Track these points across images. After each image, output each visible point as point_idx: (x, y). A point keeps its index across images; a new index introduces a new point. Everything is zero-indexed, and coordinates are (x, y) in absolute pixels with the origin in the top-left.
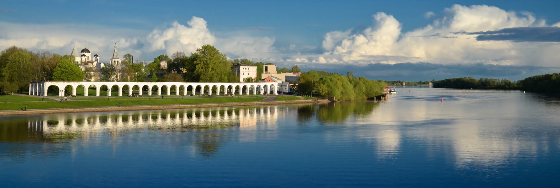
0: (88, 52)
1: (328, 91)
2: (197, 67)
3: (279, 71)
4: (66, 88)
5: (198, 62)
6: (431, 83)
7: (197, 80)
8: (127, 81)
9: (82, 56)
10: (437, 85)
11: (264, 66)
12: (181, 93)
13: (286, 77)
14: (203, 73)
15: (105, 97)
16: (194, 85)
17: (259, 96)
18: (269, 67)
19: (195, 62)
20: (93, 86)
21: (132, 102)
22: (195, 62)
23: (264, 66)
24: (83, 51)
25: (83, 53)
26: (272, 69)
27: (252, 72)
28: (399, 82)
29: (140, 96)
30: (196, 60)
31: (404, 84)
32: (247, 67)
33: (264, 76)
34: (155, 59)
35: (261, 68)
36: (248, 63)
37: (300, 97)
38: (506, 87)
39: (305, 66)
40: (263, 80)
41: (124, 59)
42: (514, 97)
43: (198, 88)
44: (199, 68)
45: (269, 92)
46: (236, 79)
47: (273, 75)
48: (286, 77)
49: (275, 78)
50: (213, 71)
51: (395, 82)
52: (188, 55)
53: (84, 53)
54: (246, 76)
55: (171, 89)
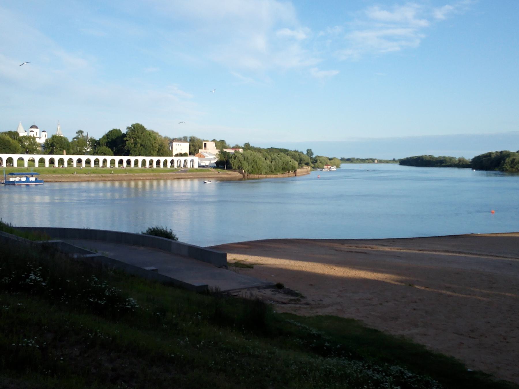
0: (37, 128)
2: (127, 143)
5: (128, 139)
7: (127, 154)
10: (404, 162)
11: (204, 143)
14: (133, 149)
15: (42, 168)
16: (125, 158)
17: (172, 168)
19: (125, 139)
20: (31, 159)
21: (48, 172)
22: (125, 139)
24: (32, 127)
25: (31, 129)
27: (185, 147)
28: (371, 159)
30: (126, 137)
31: (376, 161)
38: (461, 164)
41: (77, 135)
42: (469, 173)
43: (165, 162)
44: (130, 143)
51: (367, 159)
54: (178, 152)
55: (95, 161)
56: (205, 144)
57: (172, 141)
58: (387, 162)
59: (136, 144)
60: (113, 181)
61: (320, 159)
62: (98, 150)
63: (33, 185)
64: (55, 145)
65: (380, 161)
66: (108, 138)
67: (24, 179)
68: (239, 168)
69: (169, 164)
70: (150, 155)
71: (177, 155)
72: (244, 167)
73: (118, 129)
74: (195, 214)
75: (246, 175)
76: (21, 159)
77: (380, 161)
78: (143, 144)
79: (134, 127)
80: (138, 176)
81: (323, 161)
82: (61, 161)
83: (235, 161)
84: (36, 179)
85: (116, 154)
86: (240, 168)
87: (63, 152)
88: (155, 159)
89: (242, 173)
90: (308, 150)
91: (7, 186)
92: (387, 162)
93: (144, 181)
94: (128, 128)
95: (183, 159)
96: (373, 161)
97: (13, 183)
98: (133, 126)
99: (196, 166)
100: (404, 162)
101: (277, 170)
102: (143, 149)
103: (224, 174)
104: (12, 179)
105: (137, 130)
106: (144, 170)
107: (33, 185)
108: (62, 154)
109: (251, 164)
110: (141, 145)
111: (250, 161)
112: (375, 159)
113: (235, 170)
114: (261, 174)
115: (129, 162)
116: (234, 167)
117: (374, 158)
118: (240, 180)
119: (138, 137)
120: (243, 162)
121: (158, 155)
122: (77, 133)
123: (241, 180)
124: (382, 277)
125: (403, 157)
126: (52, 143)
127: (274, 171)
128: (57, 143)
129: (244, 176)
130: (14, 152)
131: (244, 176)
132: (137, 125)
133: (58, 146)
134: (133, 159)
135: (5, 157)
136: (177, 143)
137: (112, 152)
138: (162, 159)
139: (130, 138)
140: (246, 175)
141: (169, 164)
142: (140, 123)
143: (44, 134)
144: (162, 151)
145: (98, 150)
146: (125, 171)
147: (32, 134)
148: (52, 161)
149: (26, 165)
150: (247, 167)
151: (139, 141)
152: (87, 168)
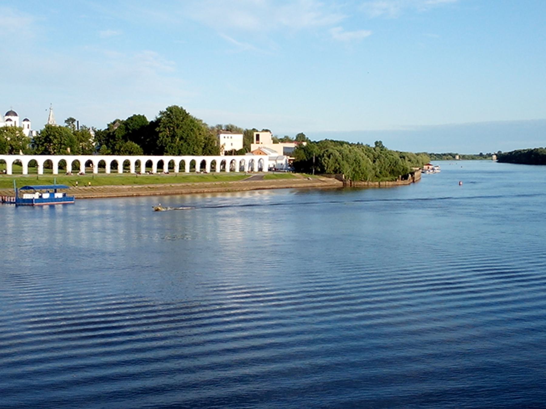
0: (16, 115)
1: (335, 168)
2: (160, 134)
3: (275, 141)
4: (125, 162)
5: (162, 130)
6: (494, 157)
8: (49, 154)
9: (7, 120)
10: (503, 158)
11: (255, 134)
12: (213, 168)
13: (284, 148)
16: (155, 159)
18: (262, 135)
19: (157, 129)
22: (157, 129)
23: (255, 134)
25: (7, 117)
26: (265, 138)
27: (235, 142)
28: (450, 154)
29: (197, 172)
31: (457, 157)
32: (230, 135)
33: (254, 147)
34: (108, 125)
35: (250, 137)
36: (230, 130)
37: (297, 174)
39: (541, 151)
40: (252, 152)
44: (164, 134)
45: (237, 170)
46: (215, 151)
47: (267, 146)
48: (284, 148)
49: (267, 149)
50: (182, 142)
51: (445, 155)
52: (151, 118)
53: (10, 117)
54: (228, 148)
55: (169, 163)
56: (258, 136)
57: (219, 130)
58: (473, 158)
59: (173, 136)
60: (11, 197)
61: (408, 155)
62: (121, 147)
63: (59, 208)
64: (49, 141)
65: (463, 157)
66: (127, 129)
67: (46, 196)
68: (335, 171)
69: (218, 168)
70: (194, 153)
71: (226, 154)
72: (344, 171)
73: (142, 115)
74: (251, 248)
75: (348, 182)
76: (18, 163)
77: (463, 157)
78: (185, 136)
79: (171, 111)
80: (200, 187)
81: (413, 159)
82: (62, 165)
83: (330, 160)
84: (64, 195)
85: (147, 153)
86: (337, 172)
87: (19, 151)
88: (198, 159)
89: (341, 180)
90: (376, 143)
91: (19, 207)
92: (473, 158)
93: (5, 196)
94: (161, 113)
95: (238, 158)
96: (453, 156)
97: (30, 202)
98: (170, 109)
99: (265, 169)
100: (503, 158)
101: (384, 174)
102: (185, 144)
103: (316, 182)
104: (27, 196)
105: (175, 117)
106: (202, 177)
107: (59, 208)
108: (19, 154)
109: (352, 165)
110: (181, 138)
111: (351, 161)
112: (457, 154)
113: (329, 175)
114: (365, 180)
115: (114, 165)
116: (328, 171)
117: (454, 152)
118: (339, 190)
119: (178, 126)
120: (342, 162)
121: (204, 154)
122: (66, 121)
123: (339, 190)
124: (160, 352)
125: (506, 149)
126: (47, 137)
127: (380, 175)
128: (55, 138)
129: (345, 184)
130: (131, 153)
131: (345, 184)
132: (176, 107)
133: (55, 141)
134: (166, 159)
135: (10, 159)
136: (226, 135)
137: (141, 150)
138: (209, 159)
139: (165, 127)
140: (348, 182)
141: (218, 168)
142: (177, 105)
143: (26, 123)
144: (209, 148)
145: (121, 147)
146: (176, 179)
147: (9, 124)
148: (48, 165)
149: (10, 172)
150: (347, 170)
151: (179, 132)
152: (60, 175)
